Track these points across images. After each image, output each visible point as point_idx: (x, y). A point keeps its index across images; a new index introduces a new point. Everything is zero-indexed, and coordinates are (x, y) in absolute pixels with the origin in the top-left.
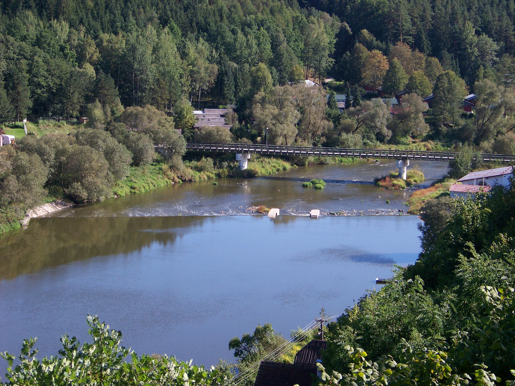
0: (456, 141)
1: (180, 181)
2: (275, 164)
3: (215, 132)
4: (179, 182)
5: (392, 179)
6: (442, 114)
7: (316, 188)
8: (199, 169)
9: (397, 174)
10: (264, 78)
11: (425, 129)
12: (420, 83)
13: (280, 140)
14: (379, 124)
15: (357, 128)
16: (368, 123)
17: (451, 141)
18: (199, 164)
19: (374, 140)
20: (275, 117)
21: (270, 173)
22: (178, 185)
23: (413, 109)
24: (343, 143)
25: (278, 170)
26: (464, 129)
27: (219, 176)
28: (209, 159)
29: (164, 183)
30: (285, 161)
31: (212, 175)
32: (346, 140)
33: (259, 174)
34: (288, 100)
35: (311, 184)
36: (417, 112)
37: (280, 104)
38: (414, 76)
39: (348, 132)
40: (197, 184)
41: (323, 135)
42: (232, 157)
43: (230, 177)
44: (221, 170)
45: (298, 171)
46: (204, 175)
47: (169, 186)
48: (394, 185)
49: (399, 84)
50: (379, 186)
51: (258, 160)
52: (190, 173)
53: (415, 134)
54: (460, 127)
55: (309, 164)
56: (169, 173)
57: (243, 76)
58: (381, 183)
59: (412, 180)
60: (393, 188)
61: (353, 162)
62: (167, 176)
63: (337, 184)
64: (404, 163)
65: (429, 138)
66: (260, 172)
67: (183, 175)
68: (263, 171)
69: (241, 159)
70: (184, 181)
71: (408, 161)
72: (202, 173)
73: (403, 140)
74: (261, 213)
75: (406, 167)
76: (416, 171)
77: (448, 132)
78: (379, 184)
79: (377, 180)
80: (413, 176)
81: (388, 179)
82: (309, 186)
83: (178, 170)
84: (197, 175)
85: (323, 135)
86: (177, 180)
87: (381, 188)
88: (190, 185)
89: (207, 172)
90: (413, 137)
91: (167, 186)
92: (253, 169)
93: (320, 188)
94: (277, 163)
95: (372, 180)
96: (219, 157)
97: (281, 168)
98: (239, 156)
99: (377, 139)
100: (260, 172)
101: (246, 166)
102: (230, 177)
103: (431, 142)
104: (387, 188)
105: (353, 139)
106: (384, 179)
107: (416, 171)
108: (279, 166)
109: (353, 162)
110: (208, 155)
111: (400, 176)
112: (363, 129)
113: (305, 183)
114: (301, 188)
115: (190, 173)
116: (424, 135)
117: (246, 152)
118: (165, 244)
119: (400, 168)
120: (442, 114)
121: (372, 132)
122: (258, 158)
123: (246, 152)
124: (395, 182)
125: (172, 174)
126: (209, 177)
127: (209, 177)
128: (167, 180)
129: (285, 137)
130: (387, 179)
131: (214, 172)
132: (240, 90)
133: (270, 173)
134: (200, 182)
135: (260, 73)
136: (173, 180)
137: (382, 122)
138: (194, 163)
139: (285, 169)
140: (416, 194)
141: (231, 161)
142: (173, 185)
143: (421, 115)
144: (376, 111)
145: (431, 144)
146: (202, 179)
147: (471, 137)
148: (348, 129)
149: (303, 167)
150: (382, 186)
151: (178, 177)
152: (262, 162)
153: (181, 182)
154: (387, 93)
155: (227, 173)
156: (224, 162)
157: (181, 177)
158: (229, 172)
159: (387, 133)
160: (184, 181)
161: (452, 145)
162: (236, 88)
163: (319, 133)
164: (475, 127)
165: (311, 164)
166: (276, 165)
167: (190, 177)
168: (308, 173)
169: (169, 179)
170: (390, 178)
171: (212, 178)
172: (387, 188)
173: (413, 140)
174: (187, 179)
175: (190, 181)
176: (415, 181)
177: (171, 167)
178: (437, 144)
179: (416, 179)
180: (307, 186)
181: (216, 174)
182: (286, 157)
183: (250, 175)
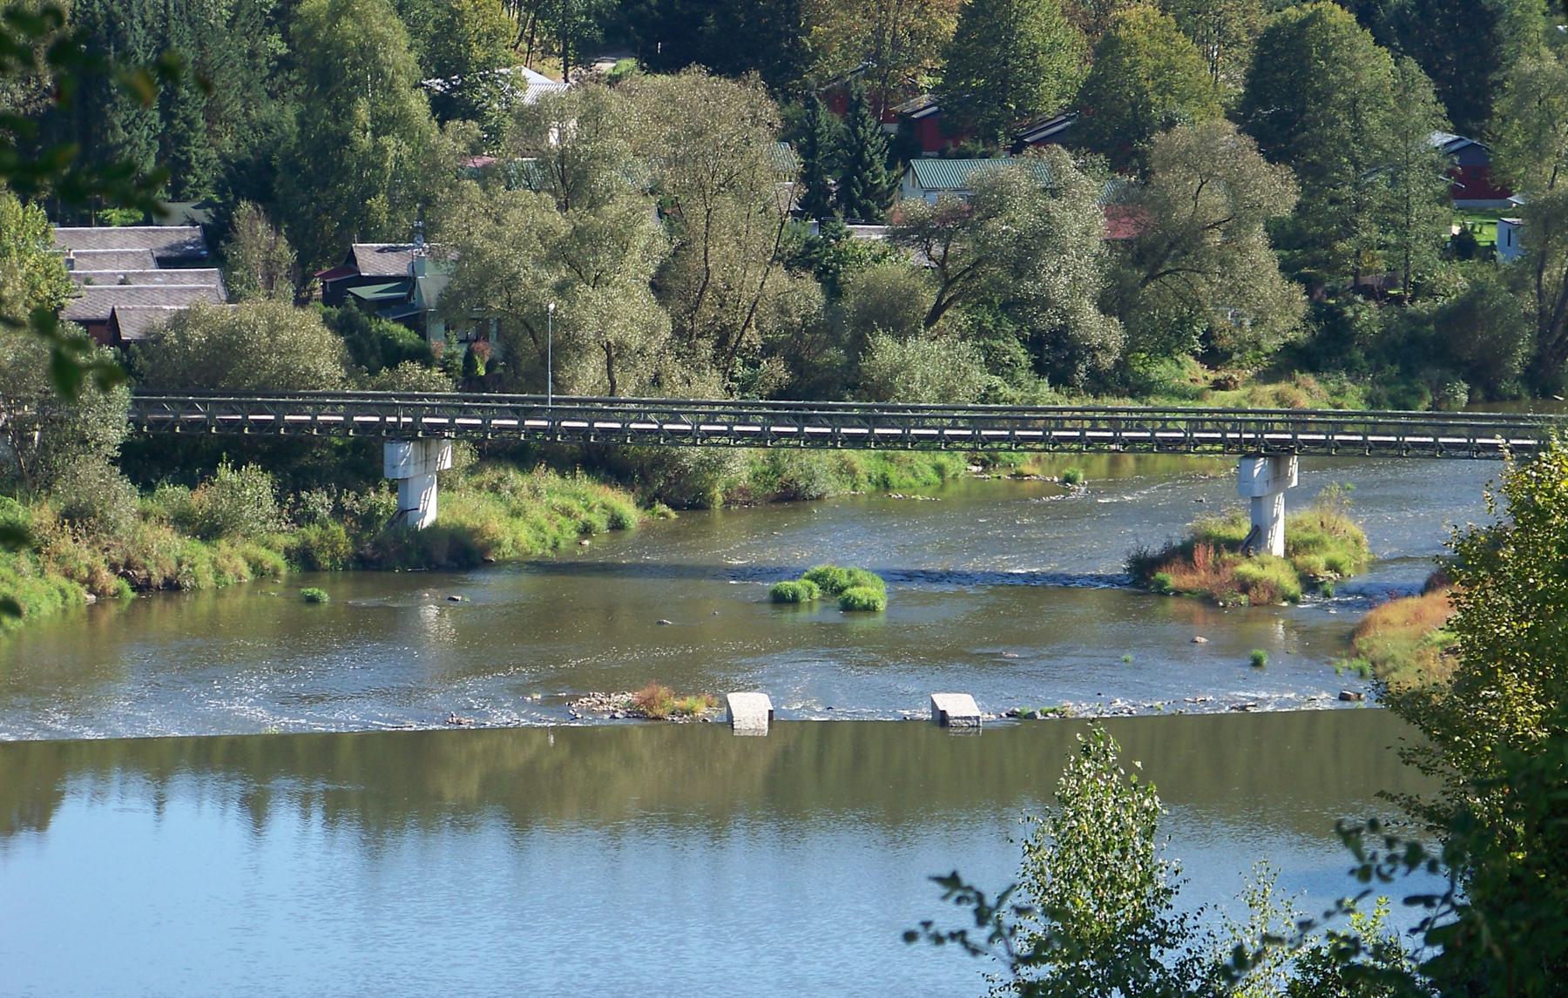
0: (1436, 373)
1: (124, 584)
2: (567, 502)
3: (262, 329)
4: (119, 592)
5: (1227, 556)
6: (1348, 230)
7: (849, 607)
8: (209, 530)
9: (1242, 531)
10: (368, 52)
11: (1283, 309)
12: (1158, 71)
13: (588, 377)
14: (1060, 285)
15: (937, 311)
16: (992, 288)
17: (1408, 373)
18: (199, 499)
19: (1022, 375)
20: (557, 254)
21: (555, 546)
22: (113, 609)
23: (1216, 201)
24: (881, 390)
25: (586, 530)
26: (1465, 312)
27: (304, 559)
28: (253, 472)
29: (50, 595)
30: (604, 482)
31: (274, 559)
32: (896, 371)
33: (507, 551)
34: (610, 160)
35: (816, 587)
36: (1234, 226)
37: (571, 180)
38: (1122, 33)
39: (900, 328)
40: (204, 604)
41: (769, 349)
42: (361, 462)
43: (364, 564)
44: (312, 533)
45: (675, 534)
46: (234, 556)
47: (72, 613)
48: (1245, 585)
49: (1036, 83)
50: (1162, 592)
51: (476, 479)
52: (167, 548)
53: (1227, 342)
54: (1441, 301)
55: (727, 503)
56: (66, 545)
57: (201, 46)
58: (1171, 578)
59: (1318, 561)
60: (1244, 598)
61: (942, 487)
62: (60, 559)
63: (936, 588)
64: (1278, 475)
65: (1294, 361)
66: (508, 540)
67: (140, 559)
68: (525, 535)
69: (412, 471)
70: (143, 587)
71: (1294, 465)
72: (223, 544)
73: (1162, 370)
74: (657, 718)
75: (1280, 499)
76: (1332, 518)
77: (1388, 327)
78: (1164, 583)
79: (1143, 570)
80: (1315, 542)
81: (1203, 555)
82: (804, 594)
83: (109, 527)
84: (200, 554)
85: (769, 349)
86: (111, 582)
87: (1172, 605)
88: (170, 609)
89: (245, 541)
90: (1213, 357)
91: (65, 611)
92: (470, 523)
93: (869, 609)
94: (577, 497)
95: (1117, 565)
96: (291, 461)
97: (600, 521)
98: (402, 456)
99: (1039, 368)
100: (508, 540)
101: (431, 511)
102: (364, 564)
103: (1310, 380)
104: (1208, 600)
105: (926, 364)
106: (1182, 554)
107: (1332, 518)
108: (590, 510)
109: (942, 487)
110: (241, 450)
111: (1257, 537)
112: (957, 316)
113: (787, 585)
114: (767, 609)
115: (167, 548)
116: (1271, 344)
117: (435, 432)
118: (373, 847)
119: (1257, 500)
120: (1348, 230)
121: (1011, 328)
122: (472, 470)
123: (435, 432)
124: (1247, 568)
125: (83, 555)
126: (257, 567)
127: (257, 567)
128: (64, 583)
129: (615, 354)
130: (1199, 555)
131: (282, 540)
132: (190, 123)
133: (555, 546)
134: (218, 593)
135: (347, 26)
136: (90, 583)
137: (1072, 282)
138: (174, 494)
139: (617, 524)
140: (1386, 622)
141: (343, 485)
142: (91, 607)
143: (1258, 237)
144: (1045, 214)
145: (1309, 393)
146: (230, 577)
147: (1509, 353)
148: (892, 314)
149: (698, 516)
150: (1178, 593)
151: (114, 567)
152: (494, 489)
153: (130, 594)
154: (973, 133)
155: (345, 545)
156: (309, 489)
157: (128, 565)
158: (356, 540)
159: (1101, 330)
160: (143, 587)
161: (1419, 395)
162: (167, 116)
163: (753, 337)
164: (1528, 303)
165: (738, 499)
166: (576, 507)
167: (170, 568)
168: (733, 544)
169: (70, 575)
170: (1218, 551)
171: (275, 573)
172: (1208, 600)
173: (1212, 375)
174: (157, 579)
175: (172, 587)
176: (1333, 566)
177: (74, 516)
178: (1340, 393)
179: (1337, 554)
180: (795, 600)
181: (288, 553)
182: (602, 460)
183: (461, 554)
